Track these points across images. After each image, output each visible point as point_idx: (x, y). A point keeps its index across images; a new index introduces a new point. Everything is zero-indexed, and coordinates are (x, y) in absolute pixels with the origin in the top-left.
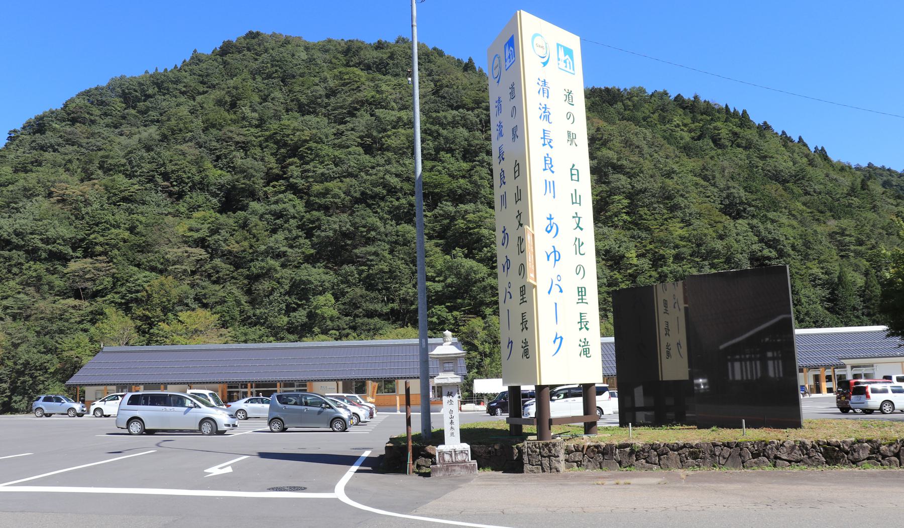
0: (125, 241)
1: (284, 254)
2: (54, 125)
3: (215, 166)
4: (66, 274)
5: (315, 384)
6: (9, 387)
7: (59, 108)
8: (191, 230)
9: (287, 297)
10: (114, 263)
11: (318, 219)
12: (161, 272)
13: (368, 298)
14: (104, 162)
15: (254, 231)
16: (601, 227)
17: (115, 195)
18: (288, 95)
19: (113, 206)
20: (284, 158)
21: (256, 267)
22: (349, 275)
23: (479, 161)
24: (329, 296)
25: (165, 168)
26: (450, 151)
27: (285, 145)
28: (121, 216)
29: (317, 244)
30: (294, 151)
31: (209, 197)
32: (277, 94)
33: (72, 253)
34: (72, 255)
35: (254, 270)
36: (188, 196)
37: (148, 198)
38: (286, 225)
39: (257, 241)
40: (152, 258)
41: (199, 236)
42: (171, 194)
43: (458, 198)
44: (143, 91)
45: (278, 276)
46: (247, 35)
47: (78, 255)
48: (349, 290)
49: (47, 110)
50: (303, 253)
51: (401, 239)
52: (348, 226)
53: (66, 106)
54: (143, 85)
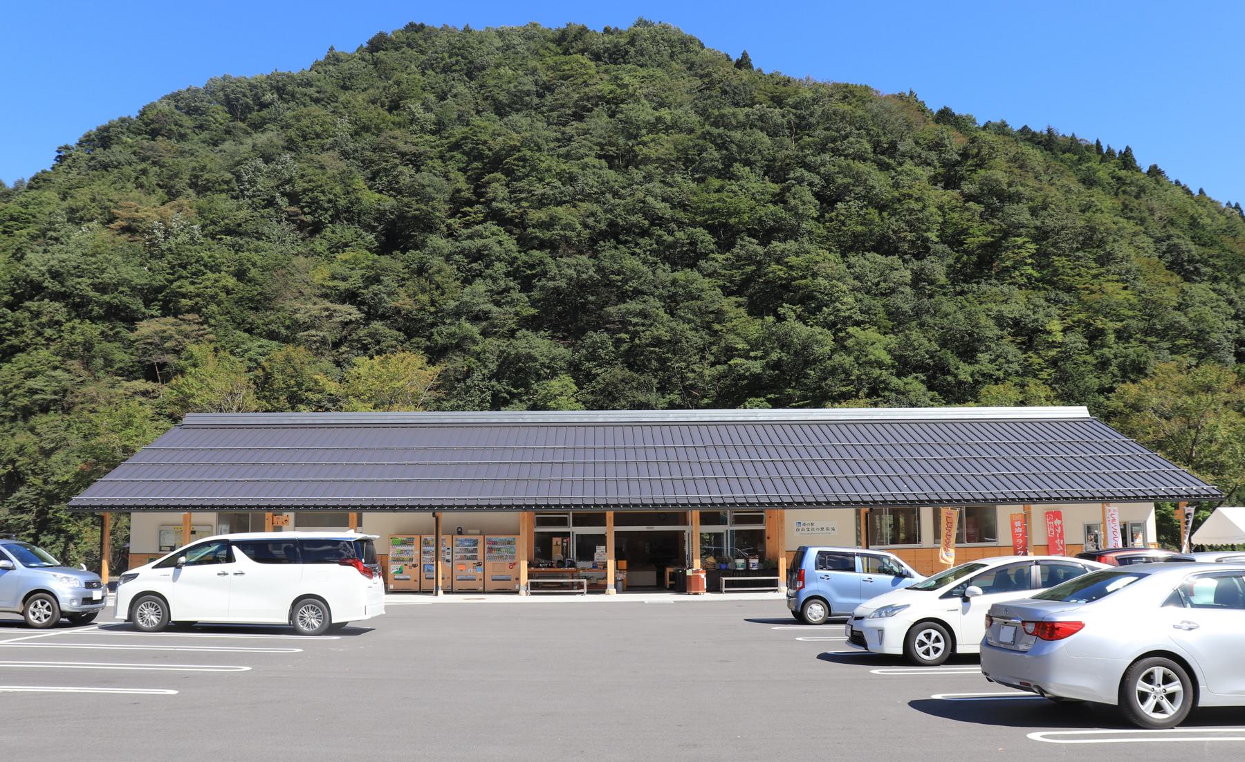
0: (228, 292)
1: (485, 316)
2: (124, 138)
3: (370, 188)
4: (134, 342)
5: (789, 514)
6: (34, 520)
7: (134, 117)
8: (334, 278)
9: (493, 382)
10: (210, 326)
11: (541, 262)
12: (286, 340)
13: (635, 384)
14: (196, 177)
15: (438, 278)
16: (996, 285)
17: (215, 223)
18: (478, 93)
19: (209, 239)
20: (480, 176)
21: (441, 335)
22: (599, 348)
23: (794, 179)
24: (567, 380)
25: (293, 186)
26: (747, 163)
27: (480, 157)
28: (221, 252)
29: (539, 301)
30: (496, 163)
31: (361, 231)
32: (460, 88)
33: (143, 310)
34: (144, 313)
35: (439, 339)
36: (328, 229)
37: (266, 230)
38: (489, 271)
39: (442, 294)
40: (272, 317)
41: (348, 286)
42: (301, 226)
43: (766, 234)
44: (257, 98)
45: (477, 348)
46: (407, 27)
47: (154, 312)
48: (599, 371)
49: (116, 119)
50: (517, 314)
51: (681, 291)
52: (591, 272)
53: (143, 113)
54: (256, 87)
